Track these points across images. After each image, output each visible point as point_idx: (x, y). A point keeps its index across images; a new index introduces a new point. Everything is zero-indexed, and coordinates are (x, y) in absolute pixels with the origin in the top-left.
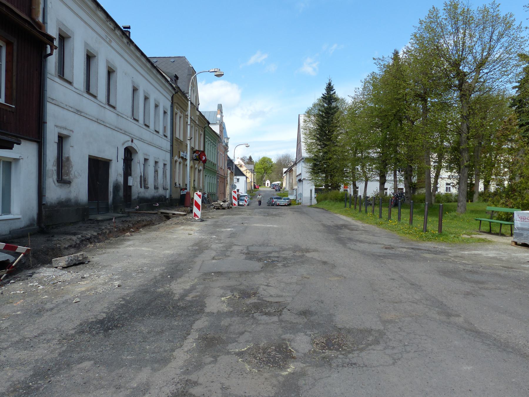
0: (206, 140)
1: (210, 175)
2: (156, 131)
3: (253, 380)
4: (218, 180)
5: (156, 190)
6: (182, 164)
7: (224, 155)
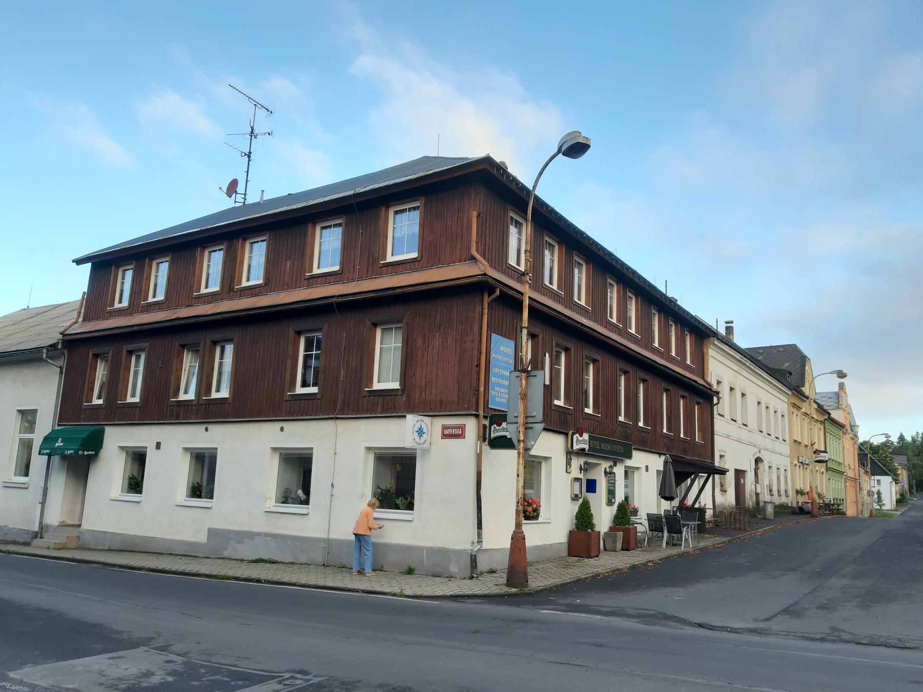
0: (827, 435)
1: (838, 478)
2: (776, 438)
3: (516, 415)
4: (847, 484)
5: (780, 497)
6: (834, 481)
7: (852, 450)
